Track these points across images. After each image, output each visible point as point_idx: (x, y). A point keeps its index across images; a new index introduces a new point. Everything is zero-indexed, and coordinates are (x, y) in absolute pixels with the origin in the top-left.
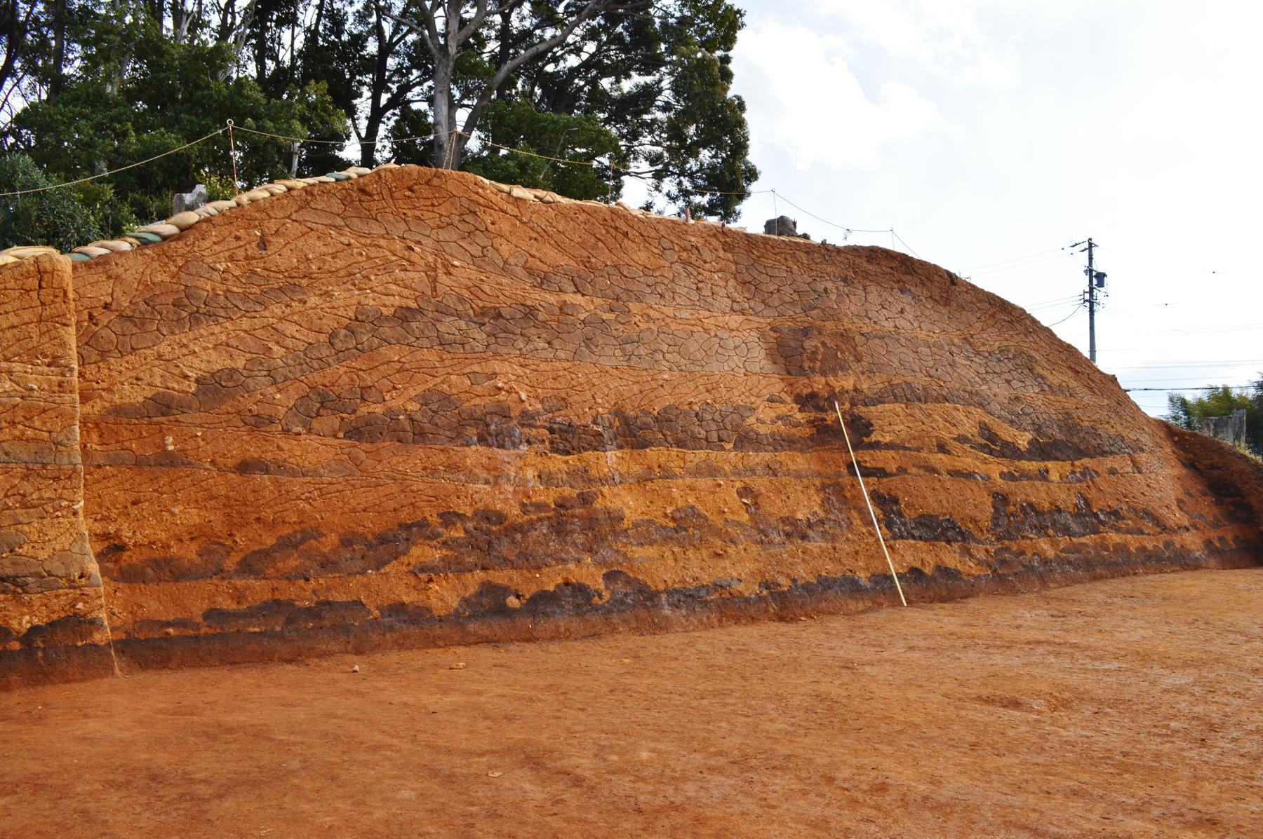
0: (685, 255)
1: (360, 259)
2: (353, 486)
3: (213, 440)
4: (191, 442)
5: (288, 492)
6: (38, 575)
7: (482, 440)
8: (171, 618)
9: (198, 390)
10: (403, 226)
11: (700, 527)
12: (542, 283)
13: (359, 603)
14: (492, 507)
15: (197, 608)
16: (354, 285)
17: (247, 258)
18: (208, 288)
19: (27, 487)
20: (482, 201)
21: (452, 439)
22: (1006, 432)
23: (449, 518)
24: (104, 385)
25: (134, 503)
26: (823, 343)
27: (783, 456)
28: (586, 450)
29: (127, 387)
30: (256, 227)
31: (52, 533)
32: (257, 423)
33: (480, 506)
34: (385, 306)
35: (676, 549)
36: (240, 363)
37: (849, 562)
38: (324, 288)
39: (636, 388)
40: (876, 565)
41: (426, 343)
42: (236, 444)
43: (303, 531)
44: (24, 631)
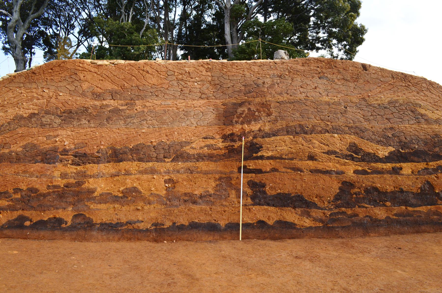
0: (180, 77)
1: (23, 97)
7: (42, 161)
12: (96, 97)
14: (35, 187)
16: (18, 107)
20: (80, 69)
22: (370, 147)
23: (17, 190)
26: (249, 109)
28: (89, 163)
33: (30, 186)
34: (26, 113)
38: (6, 109)
39: (125, 137)
40: (233, 219)
41: (35, 125)
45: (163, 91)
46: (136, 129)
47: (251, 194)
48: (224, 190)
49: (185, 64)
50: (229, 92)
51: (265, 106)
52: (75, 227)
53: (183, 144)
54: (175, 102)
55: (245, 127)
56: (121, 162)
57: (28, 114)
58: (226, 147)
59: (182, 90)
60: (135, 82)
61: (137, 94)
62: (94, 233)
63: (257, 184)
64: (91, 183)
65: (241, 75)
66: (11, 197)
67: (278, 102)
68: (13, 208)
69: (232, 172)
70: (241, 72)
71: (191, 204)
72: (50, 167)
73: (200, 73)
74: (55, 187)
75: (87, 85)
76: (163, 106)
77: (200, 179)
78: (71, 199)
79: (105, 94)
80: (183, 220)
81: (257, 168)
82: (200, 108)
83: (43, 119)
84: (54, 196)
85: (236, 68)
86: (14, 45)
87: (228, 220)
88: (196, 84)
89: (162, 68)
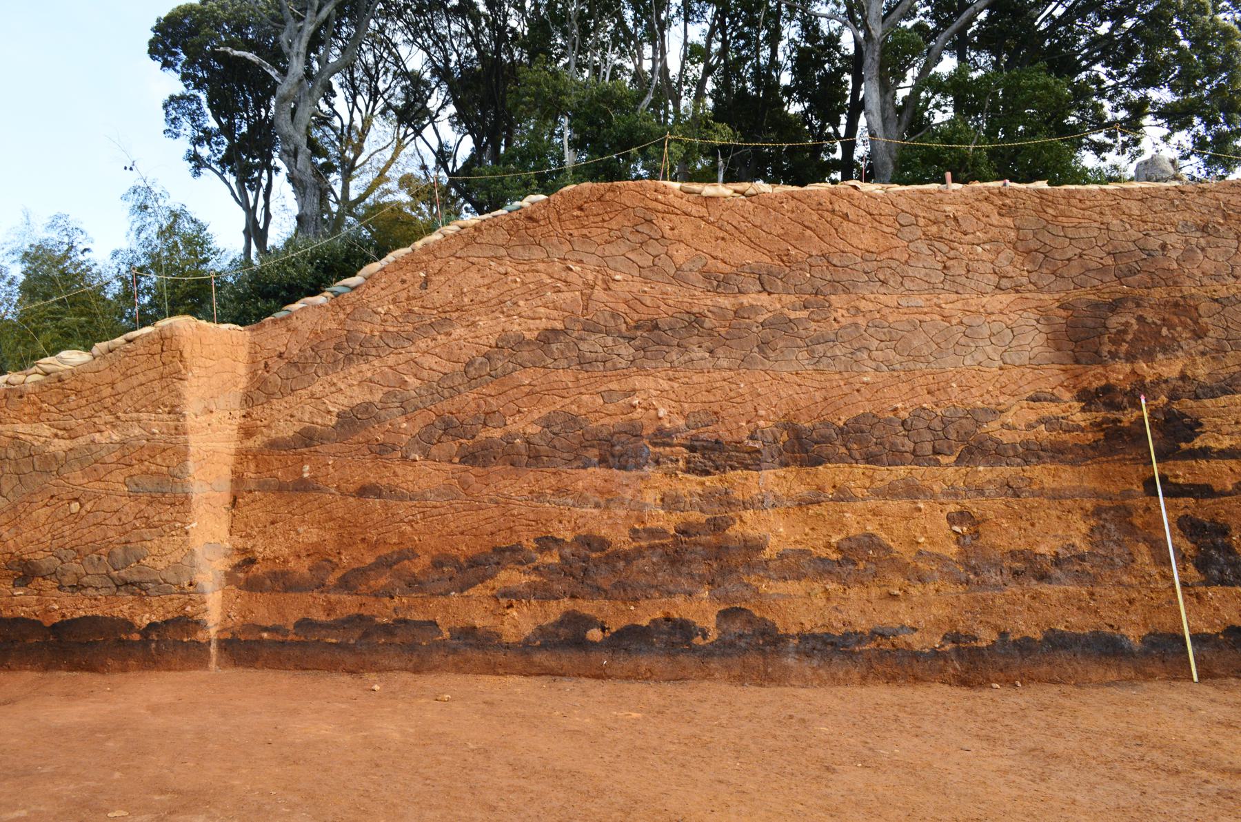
0: (934, 229)
1: (514, 285)
2: (456, 509)
3: (337, 468)
4: (323, 470)
5: (393, 515)
6: (156, 581)
7: (603, 461)
8: (270, 624)
9: (338, 422)
10: (567, 247)
11: (876, 562)
12: (718, 286)
13: (433, 623)
14: (596, 533)
15: (294, 616)
16: (503, 313)
17: (408, 299)
18: (368, 330)
19: (150, 511)
20: (660, 207)
21: (568, 462)
23: (546, 543)
24: (265, 422)
25: (272, 523)
26: (1140, 319)
27: (1036, 471)
28: (733, 468)
29: (282, 423)
30: (422, 269)
31: (168, 549)
32: (382, 451)
33: (583, 531)
34: (530, 330)
35: (831, 586)
36: (378, 396)
37: (1115, 615)
38: (472, 319)
39: (818, 396)
40: (1163, 622)
41: (564, 363)
42: (360, 471)
43: (400, 553)
44: (144, 626)
45: (898, 270)
46: (846, 375)
47: (1191, 552)
48: (1115, 542)
49: (940, 195)
50: (1074, 273)
51: (1182, 308)
52: (732, 645)
53: (981, 417)
54: (935, 300)
55: (1142, 368)
56: (820, 464)
57: (536, 333)
58: (1097, 425)
59: (945, 267)
60: (815, 247)
61: (829, 277)
62: (790, 661)
63: (1205, 526)
64: (749, 522)
65: (1096, 225)
66: (532, 560)
67: (1216, 300)
68: (545, 590)
69: (1127, 494)
70: (1096, 216)
71: (1034, 582)
72: (628, 478)
73: (985, 219)
74: (653, 533)
75: (685, 252)
76: (905, 310)
77: (1042, 514)
78: (700, 569)
79: (741, 278)
80: (1025, 626)
81: (1197, 482)
82: (1002, 317)
83: (584, 346)
84: (654, 560)
85: (1079, 205)
86: (292, 147)
87: (1146, 625)
88: (979, 249)
89: (883, 206)
